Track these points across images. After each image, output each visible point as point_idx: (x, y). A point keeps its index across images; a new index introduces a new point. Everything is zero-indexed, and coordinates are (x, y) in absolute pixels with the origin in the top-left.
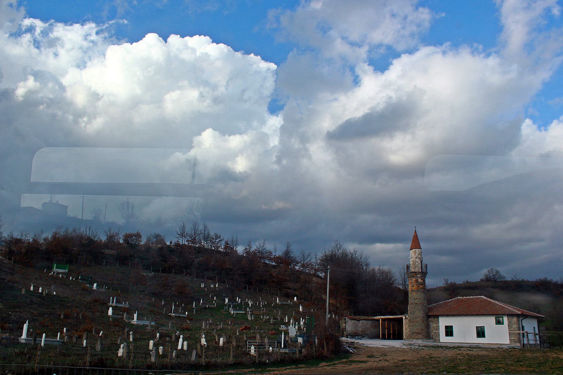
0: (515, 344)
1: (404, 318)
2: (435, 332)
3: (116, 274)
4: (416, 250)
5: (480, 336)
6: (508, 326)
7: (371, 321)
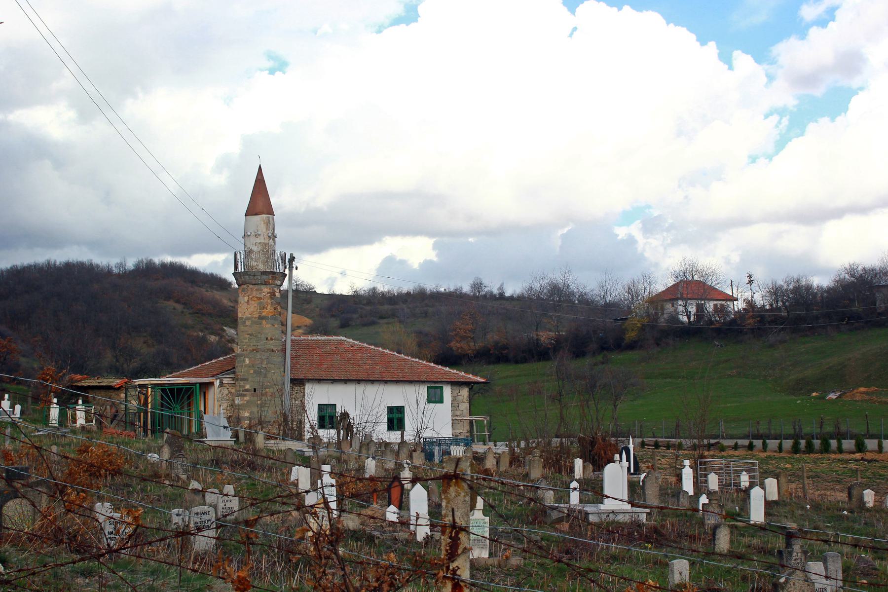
1: (217, 383)
3: (785, 298)
4: (269, 218)
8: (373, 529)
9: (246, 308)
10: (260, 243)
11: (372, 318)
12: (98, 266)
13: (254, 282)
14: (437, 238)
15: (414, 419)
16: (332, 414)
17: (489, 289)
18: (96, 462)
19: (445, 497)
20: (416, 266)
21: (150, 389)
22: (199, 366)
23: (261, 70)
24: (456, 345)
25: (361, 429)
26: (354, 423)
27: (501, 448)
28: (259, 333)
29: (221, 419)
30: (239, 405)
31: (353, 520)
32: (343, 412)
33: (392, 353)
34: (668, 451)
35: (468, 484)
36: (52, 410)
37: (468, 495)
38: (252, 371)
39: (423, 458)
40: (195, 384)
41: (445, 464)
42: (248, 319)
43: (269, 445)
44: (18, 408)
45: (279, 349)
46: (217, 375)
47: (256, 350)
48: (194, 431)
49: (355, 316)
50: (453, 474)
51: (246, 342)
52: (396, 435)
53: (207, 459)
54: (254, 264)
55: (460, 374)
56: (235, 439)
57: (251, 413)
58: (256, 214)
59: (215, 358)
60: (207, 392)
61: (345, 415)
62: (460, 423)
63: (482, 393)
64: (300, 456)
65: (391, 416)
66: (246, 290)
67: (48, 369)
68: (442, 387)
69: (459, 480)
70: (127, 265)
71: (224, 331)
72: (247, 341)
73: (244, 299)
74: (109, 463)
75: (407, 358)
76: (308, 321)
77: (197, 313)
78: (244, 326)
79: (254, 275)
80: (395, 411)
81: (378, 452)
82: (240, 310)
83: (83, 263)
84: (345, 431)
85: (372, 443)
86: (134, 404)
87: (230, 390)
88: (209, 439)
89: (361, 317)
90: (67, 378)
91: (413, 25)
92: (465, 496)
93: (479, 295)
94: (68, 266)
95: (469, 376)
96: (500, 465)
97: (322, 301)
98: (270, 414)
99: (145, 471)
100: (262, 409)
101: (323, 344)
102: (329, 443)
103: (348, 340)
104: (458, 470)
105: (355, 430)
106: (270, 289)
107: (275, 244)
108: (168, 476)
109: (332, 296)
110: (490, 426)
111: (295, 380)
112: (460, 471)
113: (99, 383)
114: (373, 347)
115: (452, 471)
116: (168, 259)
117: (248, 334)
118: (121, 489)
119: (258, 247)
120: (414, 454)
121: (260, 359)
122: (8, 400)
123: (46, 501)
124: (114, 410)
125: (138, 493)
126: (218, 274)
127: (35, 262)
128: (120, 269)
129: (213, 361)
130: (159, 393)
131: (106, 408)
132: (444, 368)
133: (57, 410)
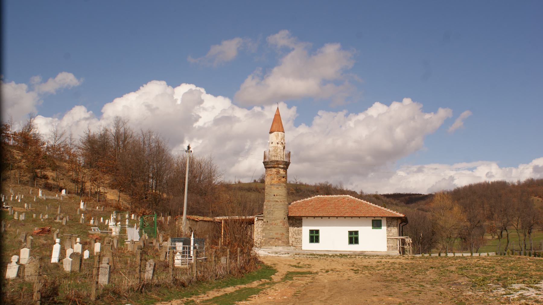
0: (393, 251)
2: (296, 237)
5: (353, 242)
6: (387, 231)
7: (208, 223)
34: (534, 258)
44: (16, 198)
65: (351, 236)
80: (354, 233)
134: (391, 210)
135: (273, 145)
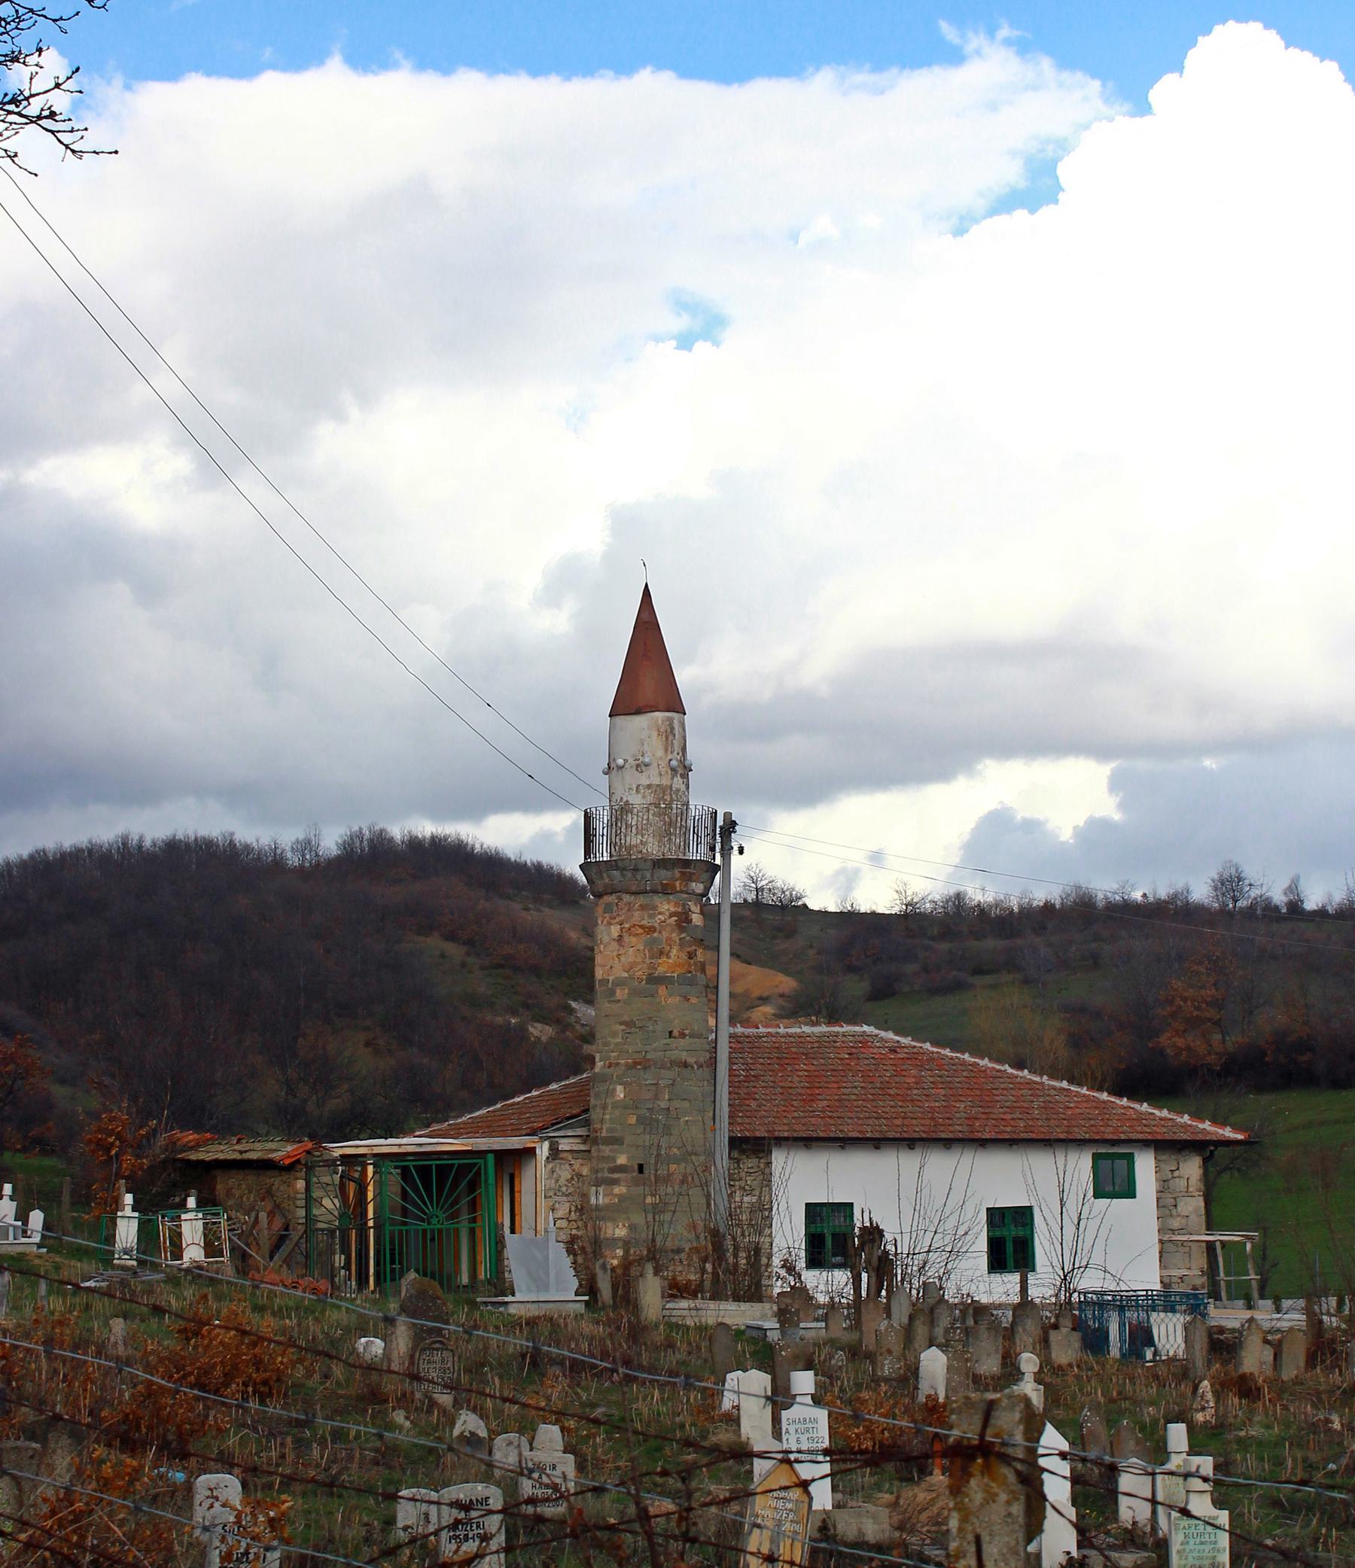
1: (543, 1150)
4: (671, 720)
8: (928, 1541)
9: (615, 953)
10: (649, 786)
11: (954, 973)
12: (248, 848)
13: (634, 888)
14: (1120, 761)
15: (1055, 1240)
16: (843, 1230)
17: (1258, 892)
18: (222, 1362)
19: (956, 1504)
20: (1066, 835)
21: (370, 1169)
22: (499, 1106)
23: (658, 339)
24: (1172, 1042)
25: (915, 1268)
26: (896, 1254)
27: (1292, 1317)
28: (650, 1018)
29: (550, 1244)
30: (597, 1208)
31: (875, 1517)
32: (868, 1225)
33: (998, 1067)
35: (1018, 1473)
36: (121, 1224)
37: (1018, 1499)
38: (633, 1120)
39: (1077, 1345)
40: (482, 1154)
41: (954, 1417)
42: (620, 983)
43: (674, 1313)
44: (37, 1218)
45: (702, 1060)
46: (542, 1129)
47: (642, 1064)
48: (482, 1276)
49: (910, 968)
50: (976, 1442)
51: (617, 1044)
52: (1009, 1286)
53: (511, 1350)
54: (635, 840)
55: (1179, 1120)
56: (586, 1298)
57: (632, 1228)
58: (639, 712)
59: (538, 1087)
60: (516, 1173)
61: (874, 1233)
62: (1181, 1249)
63: (1239, 1170)
64: (753, 1341)
66: (615, 908)
67: (112, 1119)
68: (1132, 1155)
69: (993, 1459)
70: (322, 844)
71: (572, 1011)
72: (619, 1040)
73: (609, 933)
74: (253, 1365)
75: (1038, 1079)
76: (787, 983)
77: (501, 966)
78: (609, 1002)
79: (636, 870)
81: (955, 1333)
82: (598, 959)
83: (212, 841)
84: (873, 1274)
85: (943, 1306)
86: (330, 1205)
87: (576, 1167)
88: (519, 1297)
89: (927, 971)
90: (162, 1140)
91: (1047, 212)
92: (1008, 1503)
93: (1235, 907)
94: (174, 850)
95: (1201, 1126)
96: (1281, 1365)
97: (822, 930)
98: (678, 1232)
99: (348, 1386)
100: (657, 1217)
101: (816, 1045)
102: (832, 1306)
103: (883, 1034)
104: (989, 1431)
105: (899, 1272)
106: (676, 904)
107: (688, 788)
108: (404, 1401)
109: (850, 919)
110: (1264, 1258)
111: (744, 1140)
112: (996, 1436)
113: (241, 1152)
114: (947, 1052)
115: (973, 1436)
116: (426, 828)
117: (621, 1023)
118: (281, 1433)
119: (644, 797)
120: (1053, 1335)
121: (653, 1088)
122: (12, 1198)
123: (68, 1471)
124: (278, 1223)
125: (322, 1443)
126: (553, 864)
127: (90, 842)
128: (303, 856)
129: (535, 1093)
130: (394, 1176)
131: (257, 1217)
132: (1137, 1106)
133: (135, 1224)
134: (1197, 1116)
135: (651, 777)
